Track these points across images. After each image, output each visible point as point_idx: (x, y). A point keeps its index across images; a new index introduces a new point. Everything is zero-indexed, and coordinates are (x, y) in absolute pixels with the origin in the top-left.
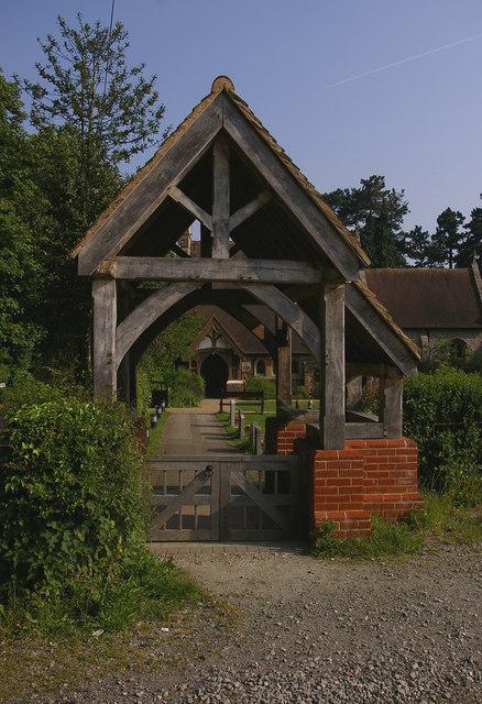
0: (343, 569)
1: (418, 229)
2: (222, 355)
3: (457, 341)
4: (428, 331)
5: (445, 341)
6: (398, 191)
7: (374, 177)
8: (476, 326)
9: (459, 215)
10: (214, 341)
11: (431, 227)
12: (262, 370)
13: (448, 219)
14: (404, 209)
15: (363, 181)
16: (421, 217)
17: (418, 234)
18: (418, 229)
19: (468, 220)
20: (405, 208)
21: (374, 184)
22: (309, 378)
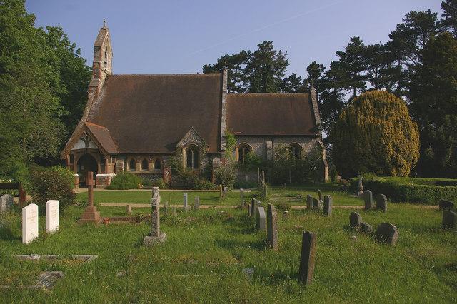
0: (314, 241)
1: (294, 75)
2: (91, 153)
3: (294, 145)
4: (272, 138)
5: (285, 145)
6: (283, 52)
7: (266, 42)
8: (310, 134)
9: (322, 66)
10: (87, 144)
11: (303, 75)
12: (133, 167)
13: (314, 69)
14: (286, 63)
15: (259, 45)
16: (297, 68)
17: (294, 79)
18: (294, 75)
19: (328, 68)
20: (287, 62)
21: (265, 47)
22: (167, 173)
